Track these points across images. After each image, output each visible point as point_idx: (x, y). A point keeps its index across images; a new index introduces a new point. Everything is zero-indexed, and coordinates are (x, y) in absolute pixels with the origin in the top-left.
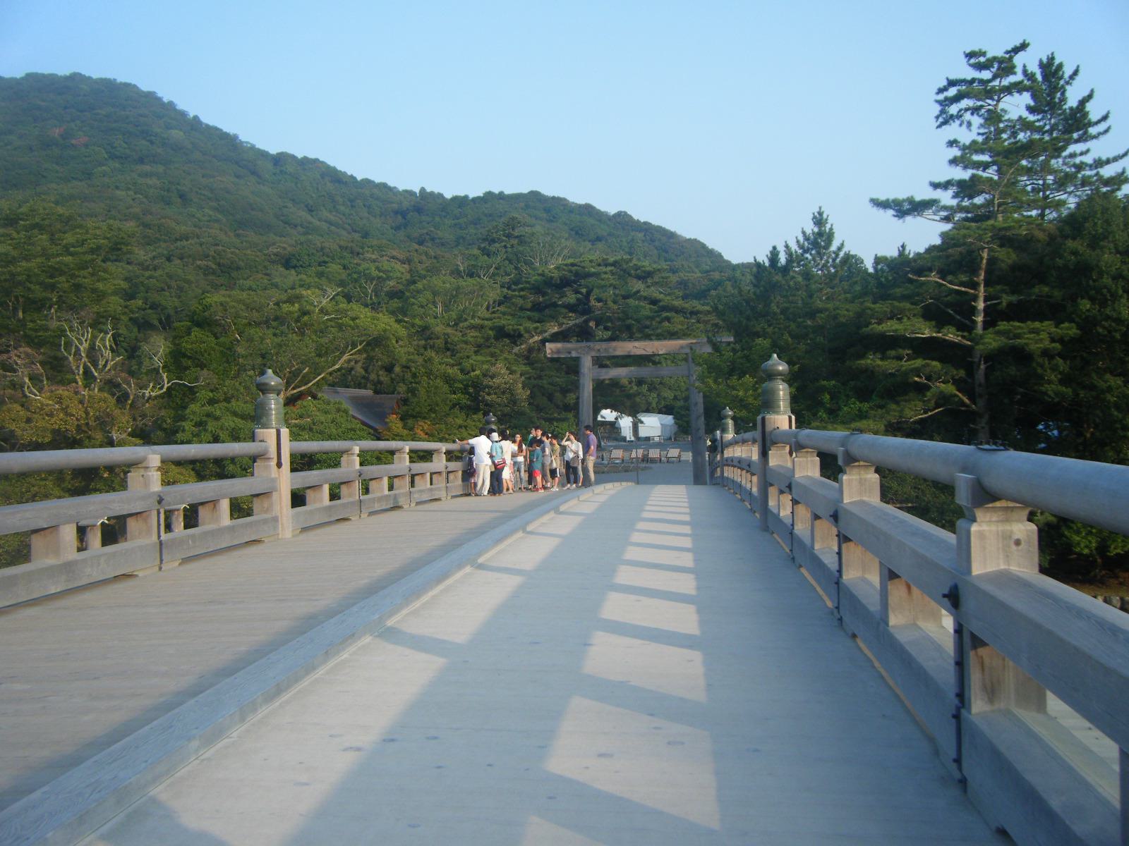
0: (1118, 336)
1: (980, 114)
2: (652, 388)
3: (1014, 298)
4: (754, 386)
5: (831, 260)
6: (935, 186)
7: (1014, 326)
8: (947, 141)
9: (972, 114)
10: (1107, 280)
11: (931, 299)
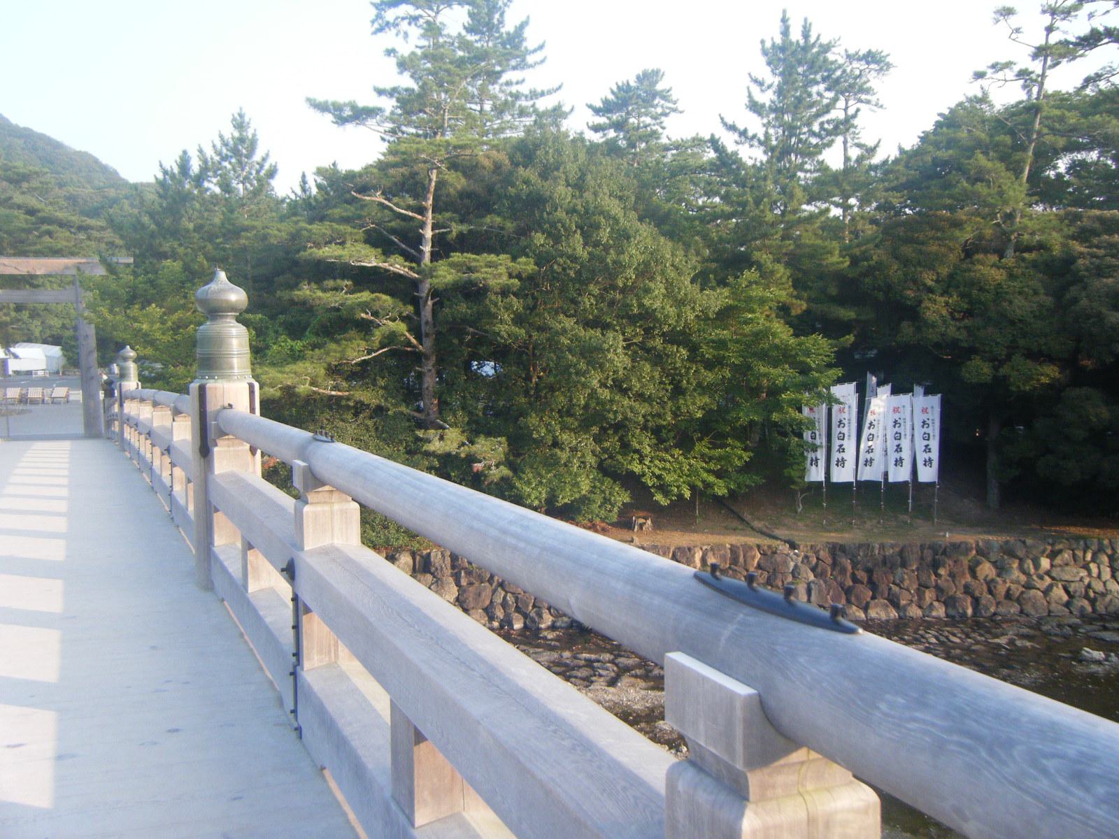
0: (572, 274)
1: (418, 24)
2: (34, 314)
3: (464, 228)
4: (161, 317)
5: (254, 172)
6: (380, 92)
7: (470, 258)
8: (384, 49)
9: (410, 24)
10: (561, 214)
11: (372, 224)
